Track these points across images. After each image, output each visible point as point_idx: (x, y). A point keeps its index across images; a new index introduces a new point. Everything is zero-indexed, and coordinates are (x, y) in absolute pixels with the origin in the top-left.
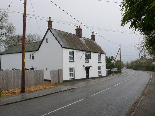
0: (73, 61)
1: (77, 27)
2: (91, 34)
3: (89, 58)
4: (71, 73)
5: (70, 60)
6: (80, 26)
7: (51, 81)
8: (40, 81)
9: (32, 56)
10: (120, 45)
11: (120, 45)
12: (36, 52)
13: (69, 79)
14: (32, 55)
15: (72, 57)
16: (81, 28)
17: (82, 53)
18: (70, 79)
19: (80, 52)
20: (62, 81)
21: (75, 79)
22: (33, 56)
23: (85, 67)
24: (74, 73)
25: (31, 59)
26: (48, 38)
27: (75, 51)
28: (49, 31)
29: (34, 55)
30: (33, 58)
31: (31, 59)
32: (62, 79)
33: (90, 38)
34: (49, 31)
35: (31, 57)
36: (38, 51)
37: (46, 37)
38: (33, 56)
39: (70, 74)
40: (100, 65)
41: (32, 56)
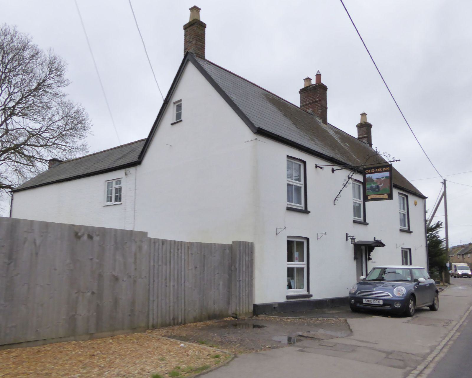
0: (302, 206)
1: (308, 79)
2: (358, 121)
3: (386, 196)
4: (293, 265)
5: (289, 199)
6: (318, 76)
7: (110, 202)
8: (116, 301)
9: (116, 190)
10: (445, 181)
11: (445, 181)
12: (132, 170)
13: (284, 300)
14: (114, 186)
15: (298, 189)
16: (323, 81)
17: (343, 174)
18: (288, 297)
19: (333, 171)
20: (251, 308)
21: (312, 298)
22: (119, 190)
23: (356, 241)
24: (305, 267)
25: (113, 202)
26: (183, 103)
27: (311, 161)
28: (191, 68)
29: (124, 186)
30: (118, 198)
31: (113, 202)
32: (250, 294)
33: (354, 133)
34: (191, 68)
35: (109, 192)
36: (139, 168)
37: (176, 98)
38: (120, 189)
39: (290, 272)
40: (408, 241)
41: (116, 190)
